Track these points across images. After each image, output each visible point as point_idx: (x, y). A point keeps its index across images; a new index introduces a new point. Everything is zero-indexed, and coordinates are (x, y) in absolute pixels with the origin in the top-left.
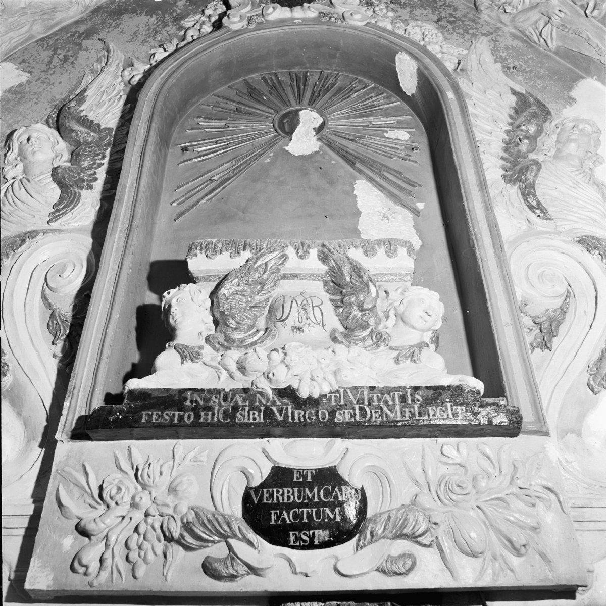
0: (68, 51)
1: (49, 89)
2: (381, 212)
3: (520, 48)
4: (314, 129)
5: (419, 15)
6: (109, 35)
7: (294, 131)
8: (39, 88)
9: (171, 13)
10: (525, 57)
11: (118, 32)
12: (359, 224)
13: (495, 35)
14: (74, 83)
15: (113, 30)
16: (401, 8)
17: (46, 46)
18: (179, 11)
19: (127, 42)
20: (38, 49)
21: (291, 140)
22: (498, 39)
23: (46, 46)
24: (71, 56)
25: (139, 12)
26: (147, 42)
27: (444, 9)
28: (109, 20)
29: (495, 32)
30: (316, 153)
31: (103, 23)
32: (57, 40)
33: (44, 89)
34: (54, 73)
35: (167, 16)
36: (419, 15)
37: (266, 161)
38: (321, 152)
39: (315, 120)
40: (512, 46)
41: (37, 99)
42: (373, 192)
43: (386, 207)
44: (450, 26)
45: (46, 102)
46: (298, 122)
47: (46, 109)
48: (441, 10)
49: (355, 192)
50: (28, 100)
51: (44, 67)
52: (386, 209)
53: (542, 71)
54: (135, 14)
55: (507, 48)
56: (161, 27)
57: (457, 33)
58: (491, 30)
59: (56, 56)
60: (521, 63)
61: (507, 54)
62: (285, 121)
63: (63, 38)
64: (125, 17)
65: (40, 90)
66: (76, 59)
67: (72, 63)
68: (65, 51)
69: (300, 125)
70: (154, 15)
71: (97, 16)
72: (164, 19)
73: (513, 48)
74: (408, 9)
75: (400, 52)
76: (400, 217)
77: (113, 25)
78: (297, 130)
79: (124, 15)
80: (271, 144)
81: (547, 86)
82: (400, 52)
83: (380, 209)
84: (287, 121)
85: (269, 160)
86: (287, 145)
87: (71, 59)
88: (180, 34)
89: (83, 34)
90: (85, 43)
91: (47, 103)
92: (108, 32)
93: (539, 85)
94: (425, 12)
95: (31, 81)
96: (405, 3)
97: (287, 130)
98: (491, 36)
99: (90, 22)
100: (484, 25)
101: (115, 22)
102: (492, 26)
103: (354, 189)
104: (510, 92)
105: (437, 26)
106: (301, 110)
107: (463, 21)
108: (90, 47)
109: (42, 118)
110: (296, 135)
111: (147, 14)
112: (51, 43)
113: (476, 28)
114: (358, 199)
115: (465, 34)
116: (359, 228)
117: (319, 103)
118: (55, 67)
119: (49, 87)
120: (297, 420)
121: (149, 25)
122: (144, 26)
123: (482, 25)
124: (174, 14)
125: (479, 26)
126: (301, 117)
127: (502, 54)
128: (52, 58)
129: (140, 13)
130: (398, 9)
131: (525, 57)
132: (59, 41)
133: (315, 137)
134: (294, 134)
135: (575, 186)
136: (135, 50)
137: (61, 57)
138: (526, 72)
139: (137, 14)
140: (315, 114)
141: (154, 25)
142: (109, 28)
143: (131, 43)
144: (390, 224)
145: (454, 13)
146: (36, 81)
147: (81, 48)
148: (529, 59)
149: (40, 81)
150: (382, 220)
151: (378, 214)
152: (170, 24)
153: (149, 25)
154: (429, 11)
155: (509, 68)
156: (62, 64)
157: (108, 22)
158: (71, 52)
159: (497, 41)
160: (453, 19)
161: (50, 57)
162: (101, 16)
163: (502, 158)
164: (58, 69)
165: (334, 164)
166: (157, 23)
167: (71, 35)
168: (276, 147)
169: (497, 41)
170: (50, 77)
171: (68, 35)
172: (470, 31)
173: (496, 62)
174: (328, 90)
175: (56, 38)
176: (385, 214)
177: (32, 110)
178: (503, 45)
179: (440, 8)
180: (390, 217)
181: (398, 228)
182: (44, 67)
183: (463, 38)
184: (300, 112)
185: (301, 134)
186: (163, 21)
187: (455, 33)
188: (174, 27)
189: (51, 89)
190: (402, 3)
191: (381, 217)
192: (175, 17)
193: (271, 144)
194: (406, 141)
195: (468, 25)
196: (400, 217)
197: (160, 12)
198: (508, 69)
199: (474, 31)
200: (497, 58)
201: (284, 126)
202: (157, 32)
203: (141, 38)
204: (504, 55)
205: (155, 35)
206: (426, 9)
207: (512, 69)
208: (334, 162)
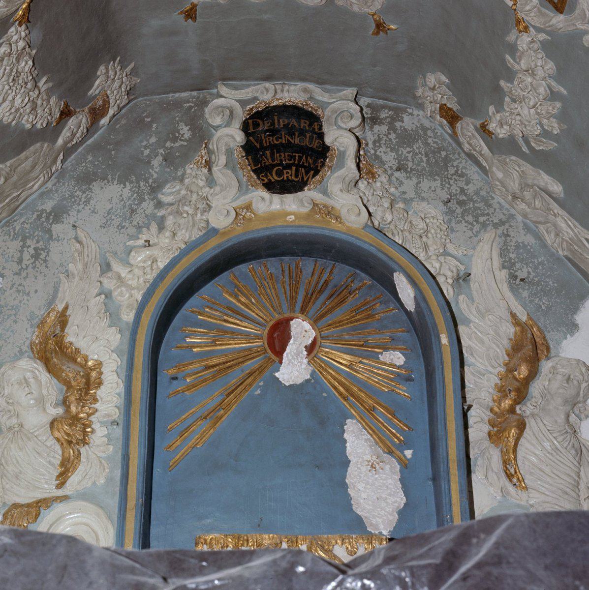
0: (38, 242)
1: (25, 301)
2: (369, 461)
3: (531, 247)
4: (306, 347)
5: (426, 190)
6: (80, 216)
7: (284, 350)
8: (14, 299)
9: (147, 181)
10: (536, 261)
11: (90, 211)
12: (348, 476)
13: (507, 226)
14: (51, 292)
15: (83, 208)
16: (407, 178)
17: (12, 234)
18: (155, 176)
19: (101, 226)
20: (5, 238)
21: (281, 363)
22: (511, 233)
23: (12, 234)
24: (43, 249)
25: (110, 177)
26: (123, 227)
27: (456, 180)
28: (78, 192)
29: (507, 221)
30: (307, 381)
31: (72, 196)
32: (23, 223)
33: (20, 302)
34: (27, 277)
35: (142, 183)
36: (426, 190)
37: (256, 393)
38: (313, 381)
39: (307, 334)
40: (523, 243)
41: (15, 315)
42: (364, 435)
43: (374, 455)
44: (459, 210)
45: (25, 319)
46: (289, 338)
47: (26, 330)
48: (451, 182)
49: (345, 435)
50: (6, 317)
51: (16, 268)
52: (374, 458)
53: (551, 283)
54: (106, 181)
55: (517, 247)
56: (136, 202)
57: (466, 222)
58: (504, 218)
59: (25, 249)
60: (530, 270)
61: (517, 254)
62: (275, 335)
63: (30, 221)
64: (95, 186)
65: (17, 302)
66: (48, 252)
67: (45, 261)
68: (35, 241)
69: (291, 342)
70: (127, 184)
71: (64, 184)
72: (139, 190)
73: (525, 246)
74: (415, 180)
75: (398, 273)
76: (387, 467)
77: (83, 200)
78: (288, 348)
79: (94, 183)
80: (261, 370)
81: (552, 306)
82: (398, 273)
83: (368, 457)
84: (278, 336)
85: (259, 392)
86: (278, 370)
87: (44, 254)
88: (158, 214)
89: (50, 214)
90: (57, 229)
91: (26, 322)
92: (79, 211)
93: (544, 303)
94: (434, 184)
95: (5, 288)
96: (412, 170)
97: (277, 348)
98: (503, 227)
99: (56, 195)
100: (497, 210)
101: (85, 195)
102: (505, 212)
103: (344, 431)
104: (510, 318)
105: (444, 208)
106: (292, 319)
107: (474, 202)
108: (61, 236)
109: (24, 343)
110: (287, 354)
111: (120, 183)
112: (17, 228)
113: (488, 214)
114: (348, 445)
115: (475, 223)
116: (347, 481)
117: (313, 310)
118: (27, 267)
119: (26, 297)
120: (268, 144)
121: (122, 200)
122: (118, 201)
123: (495, 210)
124: (150, 181)
125: (492, 210)
126: (292, 329)
127: (511, 255)
128: (21, 252)
129: (112, 179)
130: (404, 180)
131: (536, 261)
132: (26, 226)
133: (307, 359)
134: (285, 355)
135: (553, 452)
136: (112, 240)
137: (32, 251)
138: (533, 285)
139: (108, 182)
140: (307, 325)
141: (129, 199)
142: (79, 204)
143: (106, 229)
144: (377, 476)
145: (466, 187)
146: (10, 289)
147: (51, 238)
148: (539, 263)
149: (14, 289)
150: (370, 471)
151: (367, 463)
152: (146, 197)
153: (122, 200)
154: (438, 183)
155: (516, 277)
156: (34, 262)
157: (76, 194)
158: (41, 243)
159: (509, 236)
160: (465, 198)
161: (19, 251)
162: (68, 185)
163: (492, 410)
164: (30, 270)
165: (325, 398)
166: (132, 195)
167: (38, 216)
168: (267, 373)
169: (509, 236)
170: (24, 283)
171: (35, 216)
172: (481, 219)
173: (504, 267)
174: (321, 291)
175: (22, 221)
176: (373, 464)
177: (12, 331)
178: (514, 240)
179: (451, 179)
180: (378, 467)
181: (385, 482)
182: (16, 268)
183: (472, 229)
184: (292, 322)
185: (292, 353)
186: (138, 194)
187: (463, 221)
188: (152, 203)
189: (28, 300)
190: (409, 170)
191: (369, 467)
192: (151, 186)
193: (261, 370)
194: (399, 367)
195: (479, 208)
196: (387, 467)
197: (134, 178)
198: (516, 282)
199: (485, 218)
200: (505, 262)
201: (274, 342)
202: (133, 211)
203: (117, 222)
204: (513, 256)
205: (131, 216)
206: (435, 180)
207: (518, 280)
208: (325, 395)
